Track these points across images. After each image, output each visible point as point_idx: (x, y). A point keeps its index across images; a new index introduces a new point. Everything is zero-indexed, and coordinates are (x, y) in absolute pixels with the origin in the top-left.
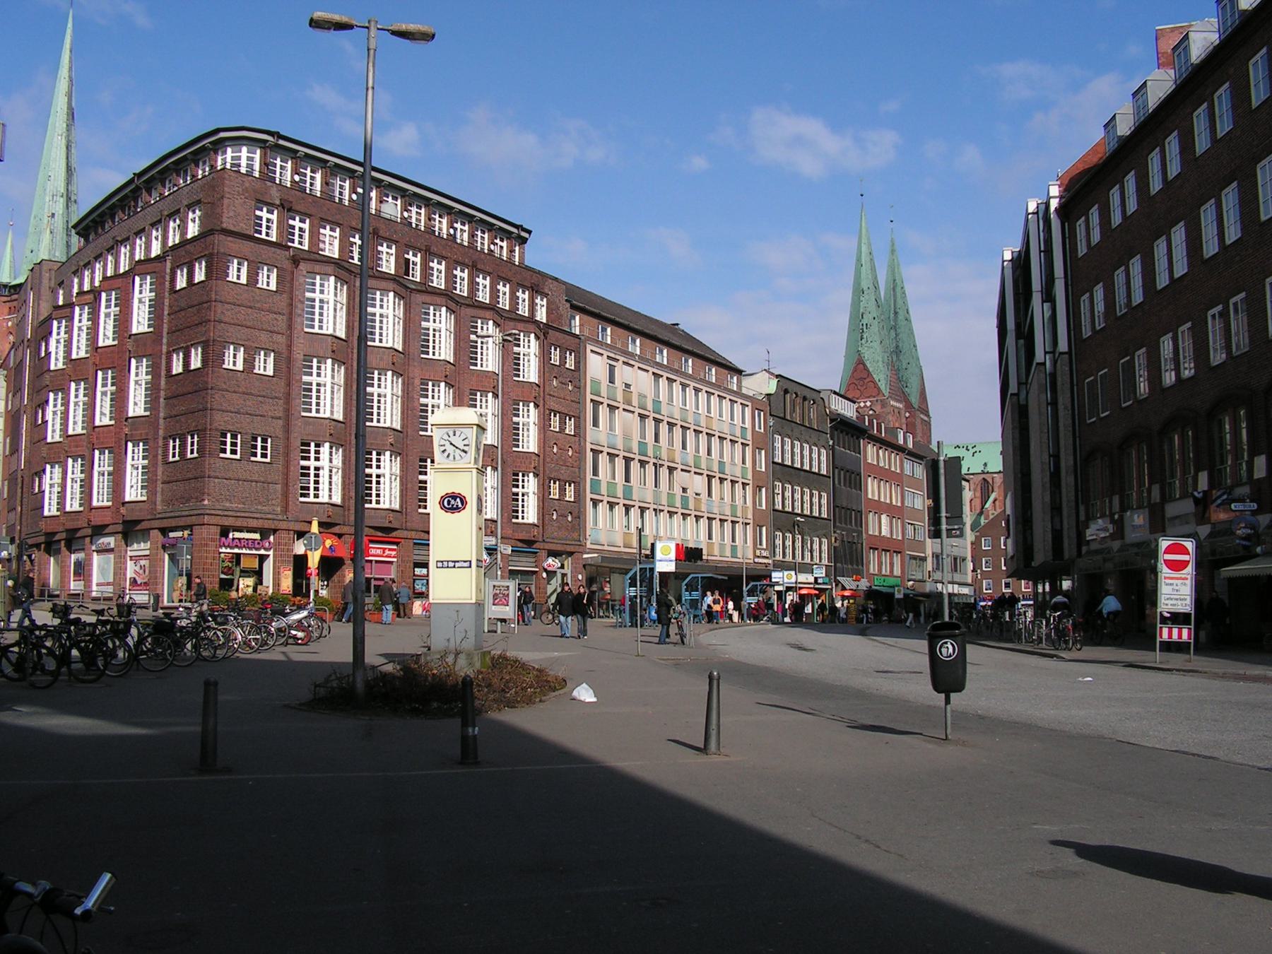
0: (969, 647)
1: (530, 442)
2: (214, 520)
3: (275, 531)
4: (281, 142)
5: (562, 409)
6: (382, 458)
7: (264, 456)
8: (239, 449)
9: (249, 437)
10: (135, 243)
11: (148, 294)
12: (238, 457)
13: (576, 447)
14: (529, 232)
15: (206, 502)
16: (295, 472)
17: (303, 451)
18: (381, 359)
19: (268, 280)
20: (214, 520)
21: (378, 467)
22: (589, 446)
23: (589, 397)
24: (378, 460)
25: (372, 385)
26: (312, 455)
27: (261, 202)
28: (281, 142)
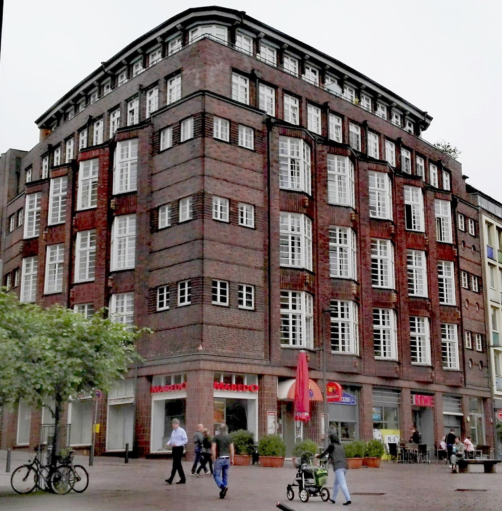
0: (111, 271)
1: (451, 298)
2: (208, 365)
3: (261, 376)
4: (245, 22)
5: (470, 270)
6: (297, 298)
7: (249, 303)
8: (253, 300)
9: (236, 287)
10: (109, 120)
11: (91, 176)
12: (227, 304)
13: (481, 304)
14: (431, 119)
15: (201, 348)
16: (276, 319)
17: (282, 300)
18: (342, 217)
19: (246, 139)
20: (208, 365)
21: (294, 307)
22: (490, 303)
23: (487, 260)
24: (294, 301)
25: (335, 241)
26: (290, 304)
27: (235, 70)
28: (245, 22)
